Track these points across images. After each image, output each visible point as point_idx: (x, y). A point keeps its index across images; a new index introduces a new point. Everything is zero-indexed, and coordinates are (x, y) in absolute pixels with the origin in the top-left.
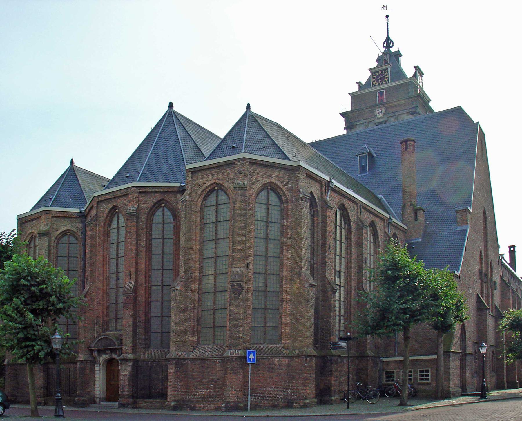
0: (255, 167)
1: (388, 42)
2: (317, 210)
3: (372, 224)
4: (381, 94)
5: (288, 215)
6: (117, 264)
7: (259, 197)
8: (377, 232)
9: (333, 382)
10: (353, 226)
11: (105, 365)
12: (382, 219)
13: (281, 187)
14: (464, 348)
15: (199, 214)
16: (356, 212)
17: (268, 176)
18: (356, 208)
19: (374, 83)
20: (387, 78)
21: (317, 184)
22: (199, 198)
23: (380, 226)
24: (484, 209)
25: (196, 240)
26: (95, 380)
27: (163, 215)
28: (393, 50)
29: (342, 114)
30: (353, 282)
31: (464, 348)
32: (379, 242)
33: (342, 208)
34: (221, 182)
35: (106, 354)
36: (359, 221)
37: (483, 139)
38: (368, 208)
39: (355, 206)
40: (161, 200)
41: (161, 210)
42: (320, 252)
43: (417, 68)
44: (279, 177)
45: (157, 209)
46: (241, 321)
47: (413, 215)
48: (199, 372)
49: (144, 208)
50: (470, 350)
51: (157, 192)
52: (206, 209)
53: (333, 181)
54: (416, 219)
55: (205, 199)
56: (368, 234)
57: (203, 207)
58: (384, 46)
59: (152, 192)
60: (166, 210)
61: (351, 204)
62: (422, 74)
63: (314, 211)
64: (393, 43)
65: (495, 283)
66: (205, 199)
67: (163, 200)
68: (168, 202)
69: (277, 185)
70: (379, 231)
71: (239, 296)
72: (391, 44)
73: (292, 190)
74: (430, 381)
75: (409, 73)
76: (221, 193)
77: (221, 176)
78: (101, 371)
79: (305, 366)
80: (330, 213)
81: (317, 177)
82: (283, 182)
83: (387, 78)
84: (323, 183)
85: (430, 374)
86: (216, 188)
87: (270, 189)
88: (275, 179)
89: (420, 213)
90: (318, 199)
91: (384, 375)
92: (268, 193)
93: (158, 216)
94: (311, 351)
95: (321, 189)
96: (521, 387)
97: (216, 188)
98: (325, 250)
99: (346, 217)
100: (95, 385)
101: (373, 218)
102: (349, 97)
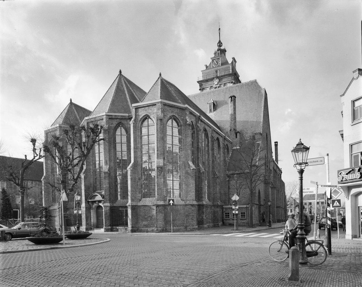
0: (166, 107)
1: (220, 44)
2: (194, 131)
3: (218, 139)
4: (217, 71)
6: (99, 156)
7: (168, 123)
8: (220, 143)
9: (204, 218)
10: (210, 139)
11: (96, 209)
12: (221, 136)
13: (178, 118)
14: (259, 201)
15: (139, 131)
16: (211, 132)
18: (211, 130)
19: (213, 66)
20: (219, 63)
21: (194, 117)
22: (139, 122)
23: (221, 140)
24: (267, 134)
25: (139, 144)
27: (121, 131)
29: (198, 82)
31: (259, 201)
33: (205, 130)
35: (96, 203)
36: (212, 137)
37: (181, 93)
38: (216, 131)
39: (210, 129)
40: (119, 123)
41: (120, 128)
42: (196, 152)
43: (234, 59)
44: (177, 113)
45: (118, 127)
47: (235, 135)
48: (143, 212)
50: (262, 203)
51: (117, 118)
53: (201, 116)
54: (236, 137)
55: (142, 123)
56: (216, 145)
58: (218, 46)
59: (115, 118)
60: (122, 128)
61: (209, 128)
62: (236, 62)
63: (193, 131)
64: (222, 44)
65: (271, 170)
67: (121, 123)
68: (123, 124)
69: (176, 117)
70: (221, 143)
72: (221, 45)
73: (183, 120)
74: (246, 218)
75: (230, 61)
76: (149, 120)
77: (150, 111)
78: (94, 212)
79: (192, 210)
81: (194, 114)
82: (179, 115)
83: (219, 63)
84: (197, 117)
85: (245, 214)
87: (173, 119)
88: (175, 114)
89: (238, 134)
90: (195, 125)
91: (225, 214)
92: (172, 121)
94: (195, 203)
97: (148, 117)
98: (199, 151)
99: (207, 135)
100: (91, 219)
101: (218, 136)
102: (201, 73)
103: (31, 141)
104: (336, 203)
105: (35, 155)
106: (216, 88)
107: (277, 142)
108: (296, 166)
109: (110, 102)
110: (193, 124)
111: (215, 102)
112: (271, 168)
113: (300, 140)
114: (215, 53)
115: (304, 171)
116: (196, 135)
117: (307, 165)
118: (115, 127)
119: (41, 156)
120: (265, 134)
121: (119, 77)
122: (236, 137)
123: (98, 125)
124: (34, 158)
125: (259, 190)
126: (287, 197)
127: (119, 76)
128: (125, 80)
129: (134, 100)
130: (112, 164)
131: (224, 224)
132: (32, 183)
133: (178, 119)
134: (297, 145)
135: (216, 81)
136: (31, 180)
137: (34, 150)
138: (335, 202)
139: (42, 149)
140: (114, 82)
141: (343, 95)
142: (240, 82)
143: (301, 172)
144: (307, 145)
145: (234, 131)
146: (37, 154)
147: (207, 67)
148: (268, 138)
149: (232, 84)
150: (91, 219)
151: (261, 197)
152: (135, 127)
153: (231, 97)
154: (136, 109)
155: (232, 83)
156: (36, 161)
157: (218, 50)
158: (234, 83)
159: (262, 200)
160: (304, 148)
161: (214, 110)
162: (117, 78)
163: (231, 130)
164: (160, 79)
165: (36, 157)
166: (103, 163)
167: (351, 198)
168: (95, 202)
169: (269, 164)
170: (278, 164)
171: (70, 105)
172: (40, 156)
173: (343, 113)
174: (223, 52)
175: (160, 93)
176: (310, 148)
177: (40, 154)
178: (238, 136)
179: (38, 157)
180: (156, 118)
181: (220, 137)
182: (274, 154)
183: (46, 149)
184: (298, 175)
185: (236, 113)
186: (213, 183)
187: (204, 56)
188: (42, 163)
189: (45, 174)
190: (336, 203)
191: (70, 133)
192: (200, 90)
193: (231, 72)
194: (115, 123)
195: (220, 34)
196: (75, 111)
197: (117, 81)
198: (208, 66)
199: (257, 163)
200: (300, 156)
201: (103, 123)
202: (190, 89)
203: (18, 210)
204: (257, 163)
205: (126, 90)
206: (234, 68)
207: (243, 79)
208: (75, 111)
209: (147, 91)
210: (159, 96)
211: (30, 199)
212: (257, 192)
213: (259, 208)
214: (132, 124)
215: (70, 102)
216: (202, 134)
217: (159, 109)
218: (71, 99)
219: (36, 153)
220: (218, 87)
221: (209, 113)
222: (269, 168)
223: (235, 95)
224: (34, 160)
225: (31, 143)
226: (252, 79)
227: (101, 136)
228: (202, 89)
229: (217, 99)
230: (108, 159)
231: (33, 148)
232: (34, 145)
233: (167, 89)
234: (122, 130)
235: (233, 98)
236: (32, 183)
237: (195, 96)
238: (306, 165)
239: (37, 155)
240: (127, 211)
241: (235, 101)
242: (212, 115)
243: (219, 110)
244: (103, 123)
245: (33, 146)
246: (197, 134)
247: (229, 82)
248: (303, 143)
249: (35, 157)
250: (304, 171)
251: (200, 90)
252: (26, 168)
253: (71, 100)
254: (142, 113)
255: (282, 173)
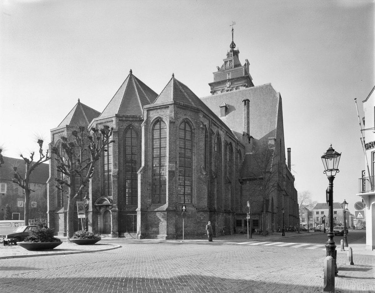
1: (233, 45)
3: (231, 144)
5: (195, 137)
9: (216, 225)
15: (151, 134)
17: (185, 115)
23: (234, 145)
26: (98, 222)
28: (235, 49)
30: (223, 174)
32: (233, 153)
34: (162, 117)
46: (174, 191)
47: (248, 140)
49: (122, 129)
50: (275, 211)
52: (154, 131)
55: (154, 126)
57: (153, 129)
58: (230, 47)
59: (125, 120)
64: (235, 46)
65: (284, 177)
66: (154, 126)
67: (131, 125)
70: (233, 147)
71: (173, 178)
75: (243, 63)
80: (213, 137)
86: (160, 120)
93: (128, 135)
95: (209, 123)
96: (163, 292)
97: (160, 120)
98: (211, 156)
103: (38, 142)
104: (360, 215)
105: (42, 157)
106: (227, 91)
107: (290, 149)
108: (326, 173)
109: (120, 104)
110: (206, 128)
111: (227, 106)
112: (284, 176)
113: (331, 145)
114: (228, 55)
115: (335, 177)
116: (209, 139)
117: (338, 171)
118: (125, 129)
119: (48, 158)
120: (279, 140)
121: (130, 77)
122: (249, 143)
123: (108, 127)
124: (41, 160)
125: (272, 198)
126: (299, 205)
127: (129, 77)
128: (136, 81)
129: (144, 102)
130: (122, 168)
131: (235, 232)
132: (35, 185)
133: (192, 123)
134: (328, 151)
135: (228, 84)
136: (34, 183)
137: (41, 151)
138: (359, 214)
139: (50, 151)
140: (124, 82)
141: (366, 101)
142: (254, 86)
143: (331, 179)
144: (337, 150)
145: (247, 136)
146: (44, 155)
147: (219, 69)
148: (282, 144)
149: (244, 88)
150: (97, 223)
151: (274, 204)
152: (146, 130)
153: (245, 101)
154: (148, 111)
155: (244, 86)
156: (41, 163)
157: (231, 51)
158: (247, 87)
159: (275, 207)
160: (335, 154)
161: (226, 114)
162: (127, 78)
163: (244, 135)
164: (172, 80)
165: (42, 158)
166: (112, 167)
167: (372, 208)
168: (103, 206)
169: (282, 171)
170: (290, 171)
171: (78, 106)
172: (47, 157)
173: (366, 120)
174: (236, 53)
175: (172, 95)
176: (342, 154)
177: (47, 155)
178: (251, 141)
179: (45, 158)
180: (168, 120)
181: (232, 142)
182: (287, 161)
183: (54, 150)
184: (328, 182)
185: (250, 118)
186: (225, 190)
187: (218, 57)
188: (47, 166)
189: (50, 177)
190: (360, 215)
191: (79, 135)
192: (211, 92)
193: (244, 75)
194: (125, 125)
195: (233, 35)
196: (83, 112)
197: (128, 81)
198: (220, 68)
199: (271, 170)
200: (331, 163)
201: (113, 125)
202: (202, 92)
203: (19, 213)
204: (271, 170)
205: (137, 91)
206: (247, 72)
207: (257, 82)
208: (83, 112)
209: (159, 94)
210: (172, 98)
211: (32, 202)
212: (270, 198)
213: (272, 216)
214: (144, 126)
215: (78, 102)
216: (215, 138)
217: (171, 112)
218: (79, 99)
219: (42, 155)
220: (230, 90)
221: (221, 116)
222: (283, 175)
223: (249, 99)
224: (41, 161)
225: (38, 144)
226: (266, 82)
227: (111, 138)
228: (213, 92)
229: (230, 104)
230: (117, 163)
231: (39, 149)
232: (41, 146)
233: (180, 90)
234: (132, 132)
235: (246, 101)
236: (35, 185)
237: (206, 99)
238: (336, 172)
239: (44, 156)
240: (136, 217)
241: (249, 105)
242: (223, 119)
243: (231, 114)
244: (113, 125)
245: (40, 147)
246: (210, 138)
247: (242, 85)
248: (334, 148)
249: (41, 158)
250: (335, 177)
251: (211, 92)
252: (33, 169)
253: (79, 100)
254: (154, 115)
255: (294, 180)
